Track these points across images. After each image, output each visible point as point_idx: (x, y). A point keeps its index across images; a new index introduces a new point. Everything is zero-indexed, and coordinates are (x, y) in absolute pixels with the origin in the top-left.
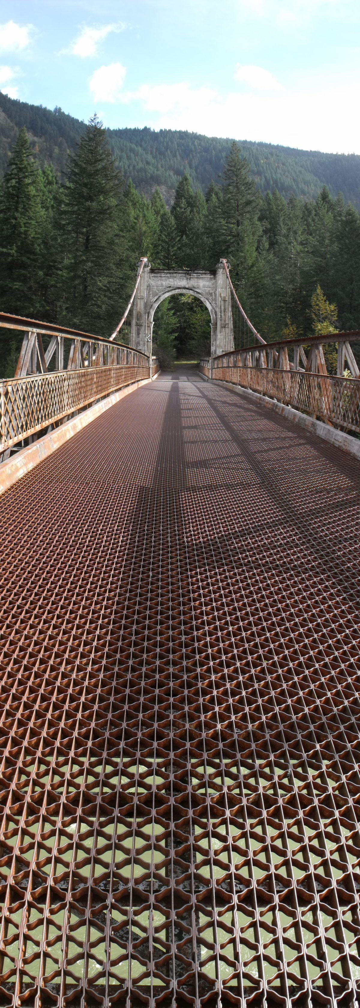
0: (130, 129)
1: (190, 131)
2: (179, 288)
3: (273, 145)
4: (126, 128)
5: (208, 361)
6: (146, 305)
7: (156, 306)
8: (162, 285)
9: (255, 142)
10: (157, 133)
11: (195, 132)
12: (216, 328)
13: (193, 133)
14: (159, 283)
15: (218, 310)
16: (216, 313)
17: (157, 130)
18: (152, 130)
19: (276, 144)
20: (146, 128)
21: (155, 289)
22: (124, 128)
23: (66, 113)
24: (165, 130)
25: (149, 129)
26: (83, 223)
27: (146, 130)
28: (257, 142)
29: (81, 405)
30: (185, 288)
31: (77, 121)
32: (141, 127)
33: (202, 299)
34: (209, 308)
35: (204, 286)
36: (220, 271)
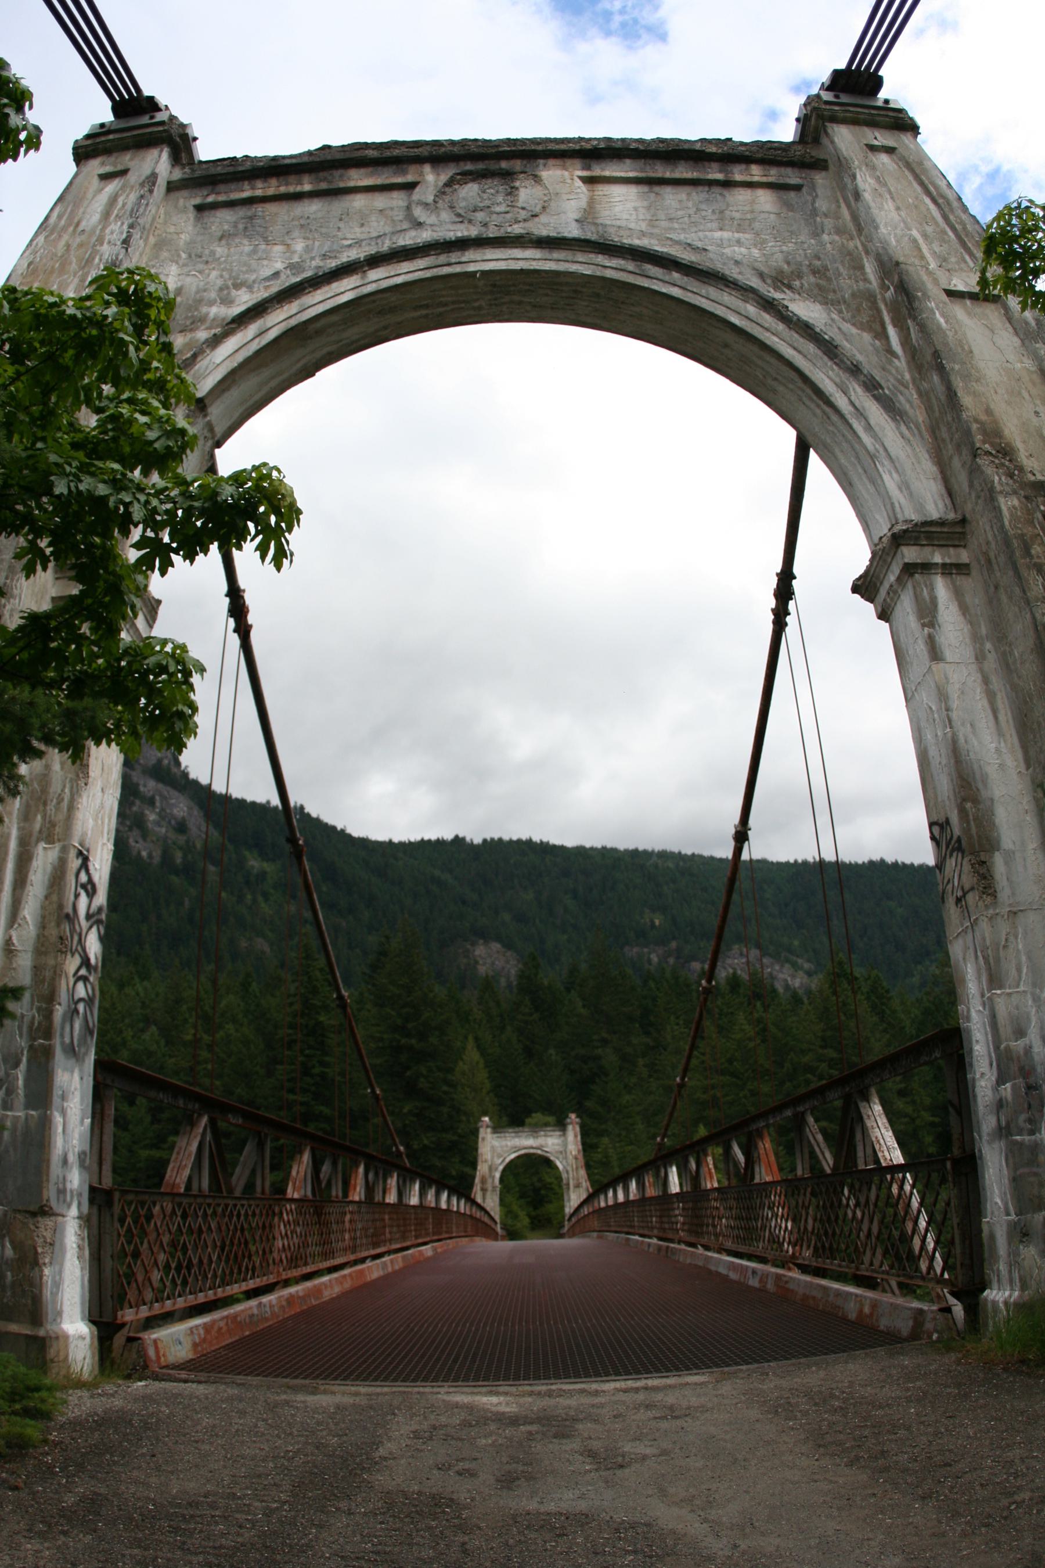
0: (429, 841)
1: (536, 839)
2: (525, 1148)
3: (686, 855)
4: (422, 840)
5: (155, 1341)
6: (490, 1168)
7: (501, 1168)
8: (507, 1146)
9: (653, 851)
10: (478, 846)
11: (545, 840)
12: (568, 1188)
13: (542, 842)
14: (504, 1143)
15: (569, 1169)
16: (567, 1172)
17: (478, 840)
18: (468, 839)
19: (689, 853)
20: (457, 837)
21: (499, 1150)
22: (419, 838)
23: (314, 815)
24: (492, 840)
25: (464, 839)
26: (402, 1148)
27: (458, 841)
28: (656, 850)
29: (201, 1298)
30: (532, 1148)
31: (334, 828)
32: (449, 836)
33: (552, 1158)
34: (560, 1167)
35: (553, 1144)
36: (570, 1127)
